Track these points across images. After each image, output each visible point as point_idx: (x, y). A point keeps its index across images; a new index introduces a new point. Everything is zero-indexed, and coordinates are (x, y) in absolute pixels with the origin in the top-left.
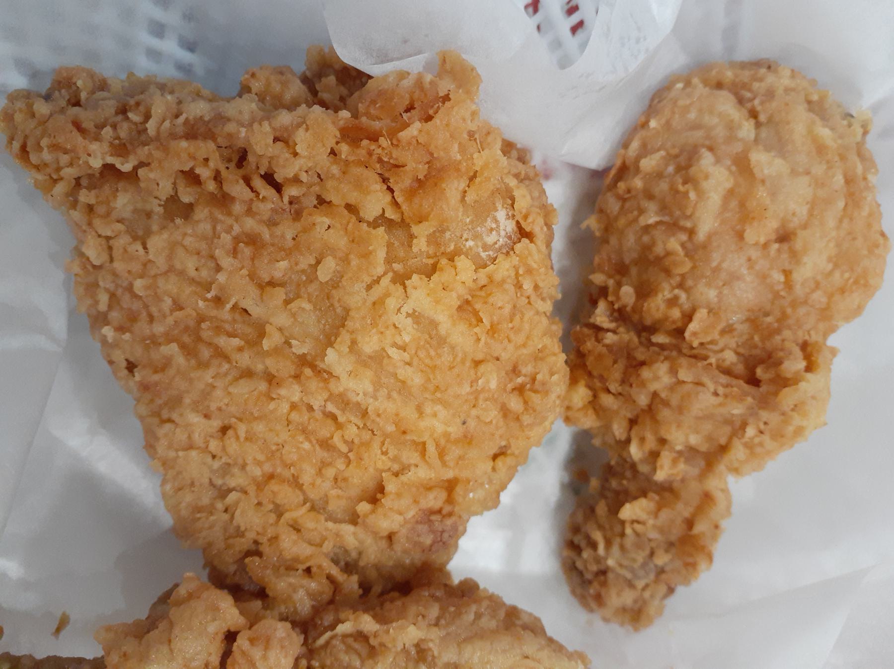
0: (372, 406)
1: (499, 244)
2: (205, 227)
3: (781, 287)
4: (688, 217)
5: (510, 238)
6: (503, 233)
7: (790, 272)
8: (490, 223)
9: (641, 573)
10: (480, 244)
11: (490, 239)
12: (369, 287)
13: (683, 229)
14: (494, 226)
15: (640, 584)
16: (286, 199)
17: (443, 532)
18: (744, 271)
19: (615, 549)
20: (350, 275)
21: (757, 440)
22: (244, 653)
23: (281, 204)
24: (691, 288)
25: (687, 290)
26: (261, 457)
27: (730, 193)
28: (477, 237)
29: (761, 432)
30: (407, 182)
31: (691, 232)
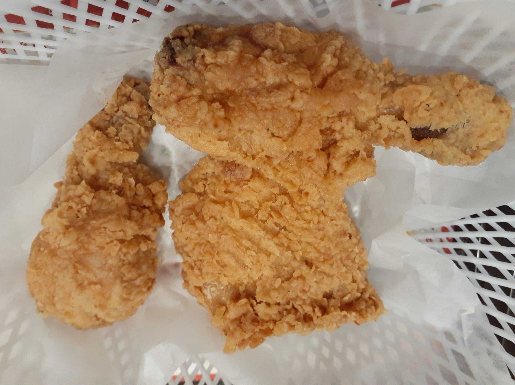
0: (262, 233)
1: (210, 286)
2: (319, 292)
3: (79, 267)
4: (125, 287)
5: (205, 288)
6: (208, 290)
7: (76, 273)
8: (214, 295)
9: (121, 121)
10: (218, 288)
11: (213, 289)
12: (226, 192)
13: (125, 281)
14: (212, 294)
15: (120, 113)
16: (291, 304)
17: (231, 175)
18: (97, 272)
19: (136, 132)
20: (270, 280)
21: (80, 206)
22: (320, 176)
23: (293, 302)
24: (120, 261)
25: (120, 260)
26: (305, 214)
27: (108, 299)
28: (219, 290)
29: (78, 211)
30: (249, 316)
31: (122, 282)
